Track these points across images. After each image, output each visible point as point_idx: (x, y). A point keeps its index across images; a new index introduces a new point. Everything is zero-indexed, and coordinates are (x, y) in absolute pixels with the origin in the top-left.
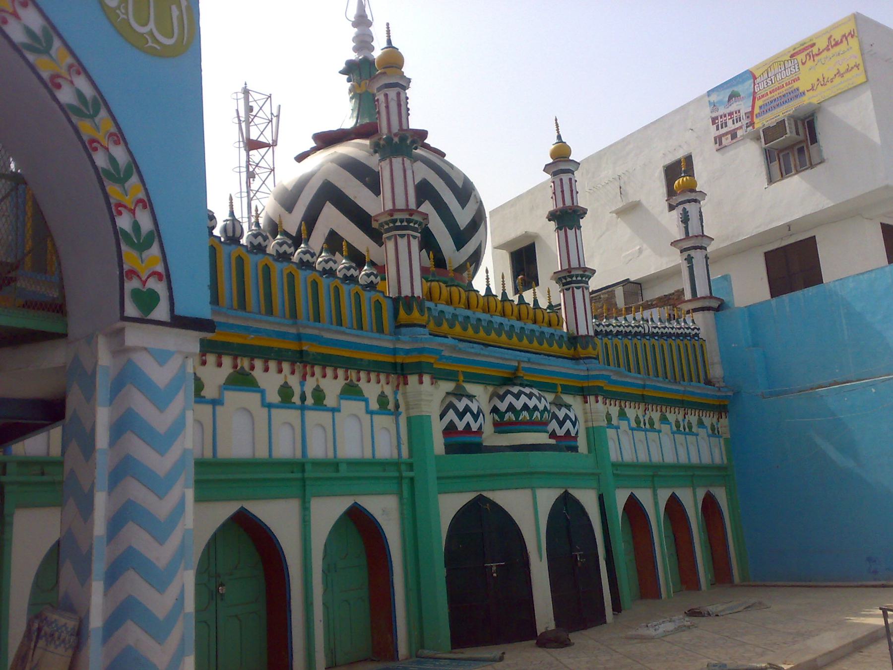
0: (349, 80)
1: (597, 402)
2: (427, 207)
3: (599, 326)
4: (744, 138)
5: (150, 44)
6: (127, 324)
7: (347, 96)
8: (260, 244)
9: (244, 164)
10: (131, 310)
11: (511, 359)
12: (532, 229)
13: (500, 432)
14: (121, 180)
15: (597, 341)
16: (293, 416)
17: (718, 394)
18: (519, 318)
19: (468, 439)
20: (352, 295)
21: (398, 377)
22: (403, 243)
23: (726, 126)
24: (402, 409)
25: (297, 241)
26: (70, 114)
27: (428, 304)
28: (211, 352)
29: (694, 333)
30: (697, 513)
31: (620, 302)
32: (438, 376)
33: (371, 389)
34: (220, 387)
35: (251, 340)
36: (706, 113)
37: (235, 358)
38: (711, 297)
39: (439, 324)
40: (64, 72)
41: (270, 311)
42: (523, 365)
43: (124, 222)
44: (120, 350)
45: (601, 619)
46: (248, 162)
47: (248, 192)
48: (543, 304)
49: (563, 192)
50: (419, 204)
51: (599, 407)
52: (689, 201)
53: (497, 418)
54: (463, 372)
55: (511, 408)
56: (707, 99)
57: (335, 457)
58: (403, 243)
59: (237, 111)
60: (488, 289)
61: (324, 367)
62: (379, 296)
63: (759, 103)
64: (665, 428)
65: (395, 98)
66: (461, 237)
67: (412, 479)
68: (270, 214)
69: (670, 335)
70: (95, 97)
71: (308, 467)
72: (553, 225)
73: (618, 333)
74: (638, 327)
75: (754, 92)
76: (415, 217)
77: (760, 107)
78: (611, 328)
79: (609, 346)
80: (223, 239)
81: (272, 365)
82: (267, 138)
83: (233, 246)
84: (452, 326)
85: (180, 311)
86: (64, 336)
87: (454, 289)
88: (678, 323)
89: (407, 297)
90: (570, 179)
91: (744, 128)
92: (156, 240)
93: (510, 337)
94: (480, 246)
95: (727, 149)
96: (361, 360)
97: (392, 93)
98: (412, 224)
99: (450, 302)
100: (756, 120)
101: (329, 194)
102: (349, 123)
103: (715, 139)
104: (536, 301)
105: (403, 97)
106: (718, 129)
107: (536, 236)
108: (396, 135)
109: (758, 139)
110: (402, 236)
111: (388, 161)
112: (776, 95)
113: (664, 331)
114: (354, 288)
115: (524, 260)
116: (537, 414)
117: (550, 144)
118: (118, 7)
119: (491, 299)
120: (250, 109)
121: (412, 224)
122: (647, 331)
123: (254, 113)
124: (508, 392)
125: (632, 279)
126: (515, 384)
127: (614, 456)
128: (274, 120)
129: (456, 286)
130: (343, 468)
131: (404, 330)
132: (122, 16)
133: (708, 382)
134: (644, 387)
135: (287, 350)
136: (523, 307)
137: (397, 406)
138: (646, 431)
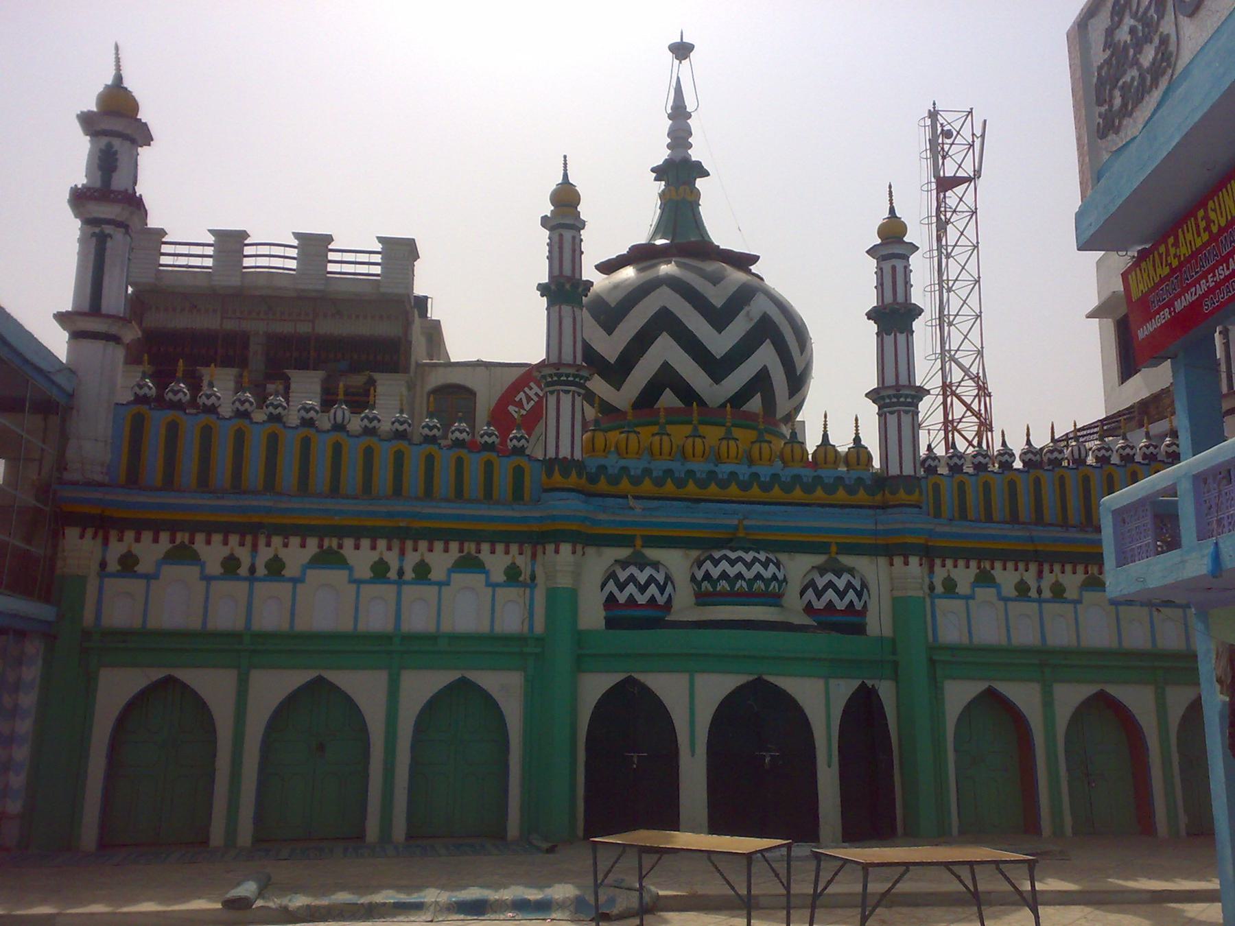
13: (705, 605)
16: (388, 591)
19: (650, 613)
24: (540, 579)
35: (337, 521)
55: (707, 576)
65: (570, 240)
82: (968, 170)
90: (574, 238)
98: (902, 399)
101: (665, 322)
137: (533, 578)
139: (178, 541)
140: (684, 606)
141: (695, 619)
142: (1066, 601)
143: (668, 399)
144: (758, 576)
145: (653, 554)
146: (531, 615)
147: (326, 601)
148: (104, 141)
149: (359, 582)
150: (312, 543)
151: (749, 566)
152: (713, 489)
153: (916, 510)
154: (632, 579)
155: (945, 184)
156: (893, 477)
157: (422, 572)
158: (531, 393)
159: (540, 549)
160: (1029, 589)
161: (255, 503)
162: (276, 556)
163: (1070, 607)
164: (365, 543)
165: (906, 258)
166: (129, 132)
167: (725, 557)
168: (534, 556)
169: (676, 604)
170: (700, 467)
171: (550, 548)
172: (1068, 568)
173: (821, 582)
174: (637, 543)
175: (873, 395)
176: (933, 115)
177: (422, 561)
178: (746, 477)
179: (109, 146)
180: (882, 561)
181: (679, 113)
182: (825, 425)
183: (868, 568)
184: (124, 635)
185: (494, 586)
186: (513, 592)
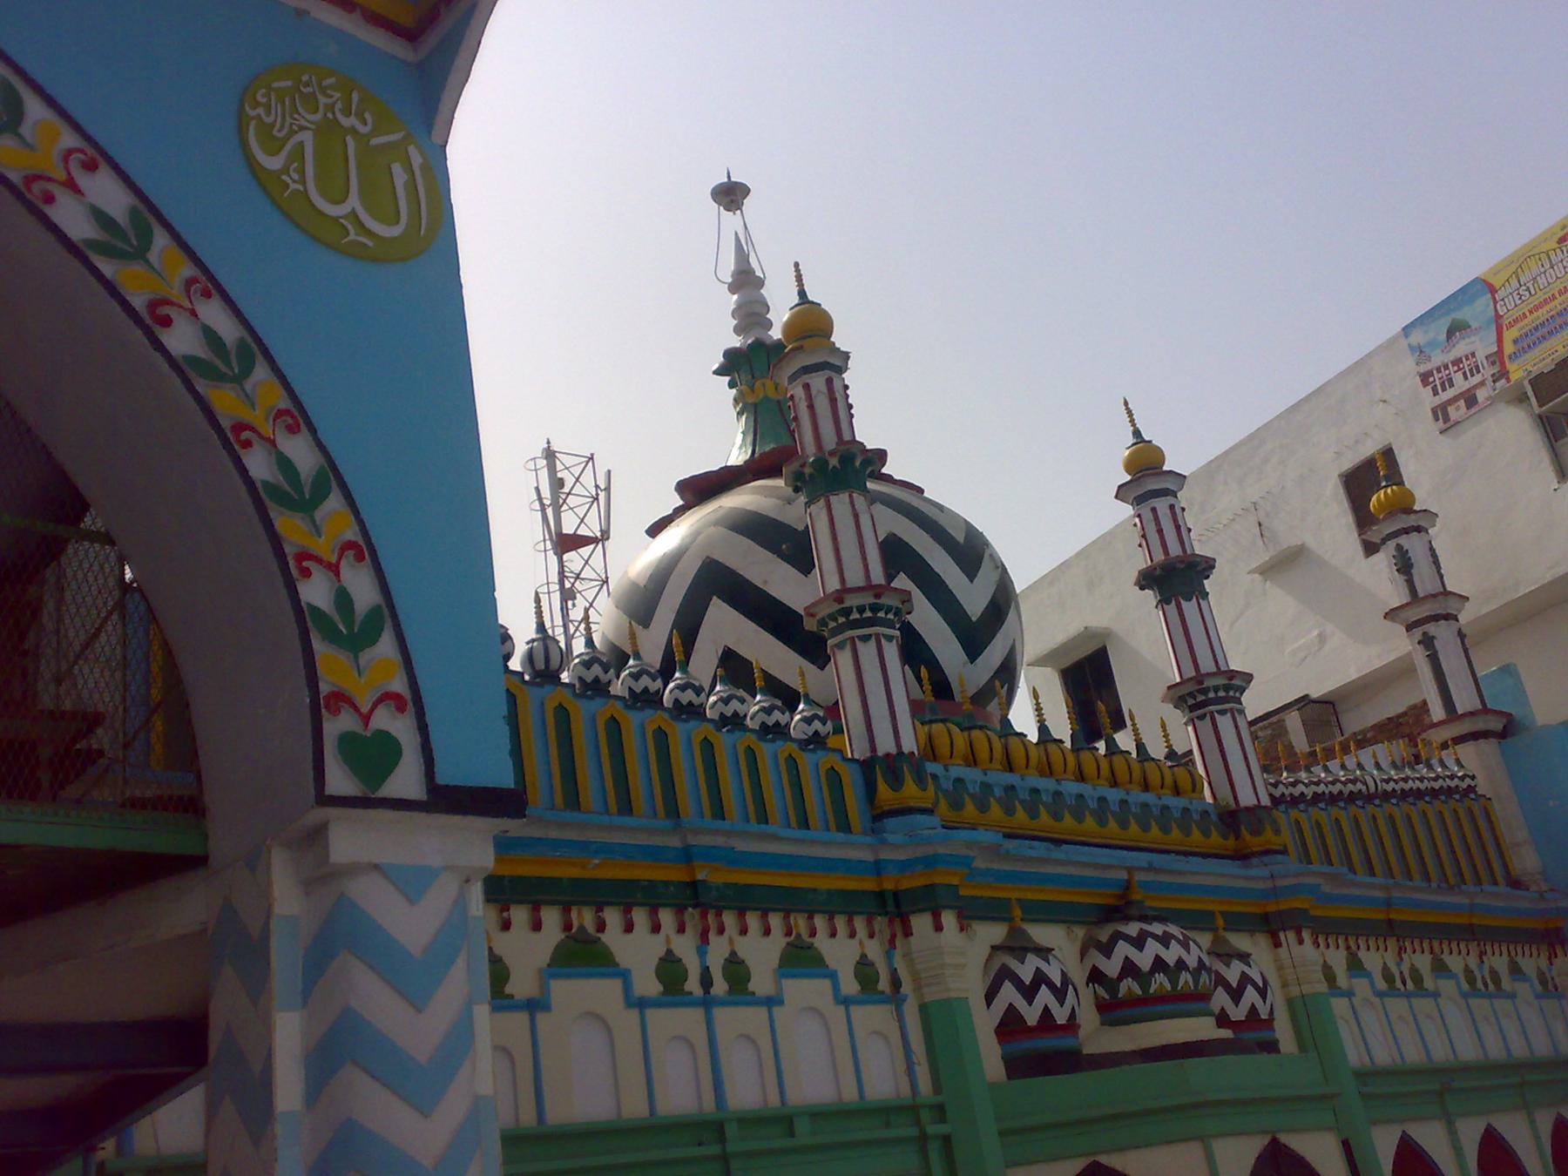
0: (731, 385)
1: (1301, 942)
2: (902, 582)
3: (1275, 785)
4: (1492, 401)
5: (352, 236)
6: (333, 812)
7: (733, 413)
8: (597, 680)
9: (554, 578)
10: (339, 781)
11: (1112, 866)
12: (1098, 621)
14: (305, 502)
15: (1279, 815)
16: (688, 1019)
17: (1542, 905)
18: (1114, 783)
20: (782, 761)
21: (891, 922)
22: (867, 652)
23: (1452, 385)
24: (906, 988)
25: (666, 673)
26: (191, 374)
27: (931, 767)
28: (521, 902)
29: (1464, 785)
30: (1545, 1166)
31: (1300, 741)
32: (970, 913)
33: (840, 950)
34: (540, 971)
36: (1409, 367)
37: (567, 910)
38: (1485, 710)
39: (957, 805)
40: (176, 292)
41: (626, 807)
42: (1140, 877)
43: (316, 592)
44: (322, 876)
46: (562, 573)
47: (565, 626)
48: (1157, 750)
49: (1160, 531)
50: (890, 577)
51: (1306, 953)
52: (1406, 531)
53: (1102, 992)
54: (1019, 900)
55: (1129, 968)
56: (1404, 343)
57: (783, 1103)
58: (867, 652)
59: (537, 489)
60: (1043, 729)
61: (741, 914)
62: (835, 759)
63: (1509, 335)
64: (1447, 986)
65: (824, 389)
66: (976, 635)
67: (947, 1140)
68: (611, 636)
69: (1419, 794)
70: (242, 340)
71: (731, 1130)
72: (1150, 596)
73: (1317, 797)
74: (1354, 781)
75: (1498, 317)
76: (886, 600)
77: (1515, 342)
78: (1301, 788)
79: (1306, 826)
80: (527, 678)
81: (640, 916)
82: (592, 528)
83: (548, 688)
84: (983, 807)
85: (443, 777)
86: (197, 862)
87: (976, 733)
88: (1430, 767)
89: (888, 755)
90: (1172, 507)
91: (1489, 383)
92: (388, 624)
93: (1102, 822)
94: (1013, 648)
95: (1458, 427)
96: (815, 890)
97: (818, 382)
98: (881, 614)
99: (972, 760)
100: (1511, 367)
101: (714, 582)
102: (737, 456)
103: (1434, 411)
104: (1140, 746)
105: (837, 385)
106: (1435, 393)
107: (1107, 634)
108: (832, 453)
109: (1522, 399)
111: (822, 502)
112: (1542, 314)
113: (1407, 786)
114: (784, 748)
115: (1090, 678)
116: (1185, 978)
117: (1122, 447)
118: (285, 170)
119: (1052, 747)
120: (557, 484)
121: (881, 614)
122: (1372, 789)
123: (566, 490)
124: (1117, 936)
125: (1315, 695)
126: (1127, 919)
127: (1354, 1056)
128: (602, 496)
129: (981, 728)
130: (802, 1126)
131: (891, 823)
132: (293, 186)
133: (1515, 884)
134: (1389, 903)
135: (667, 883)
136: (1117, 759)
137: (896, 983)
138: (1408, 995)
142: (753, 1000)
156: (1247, 809)
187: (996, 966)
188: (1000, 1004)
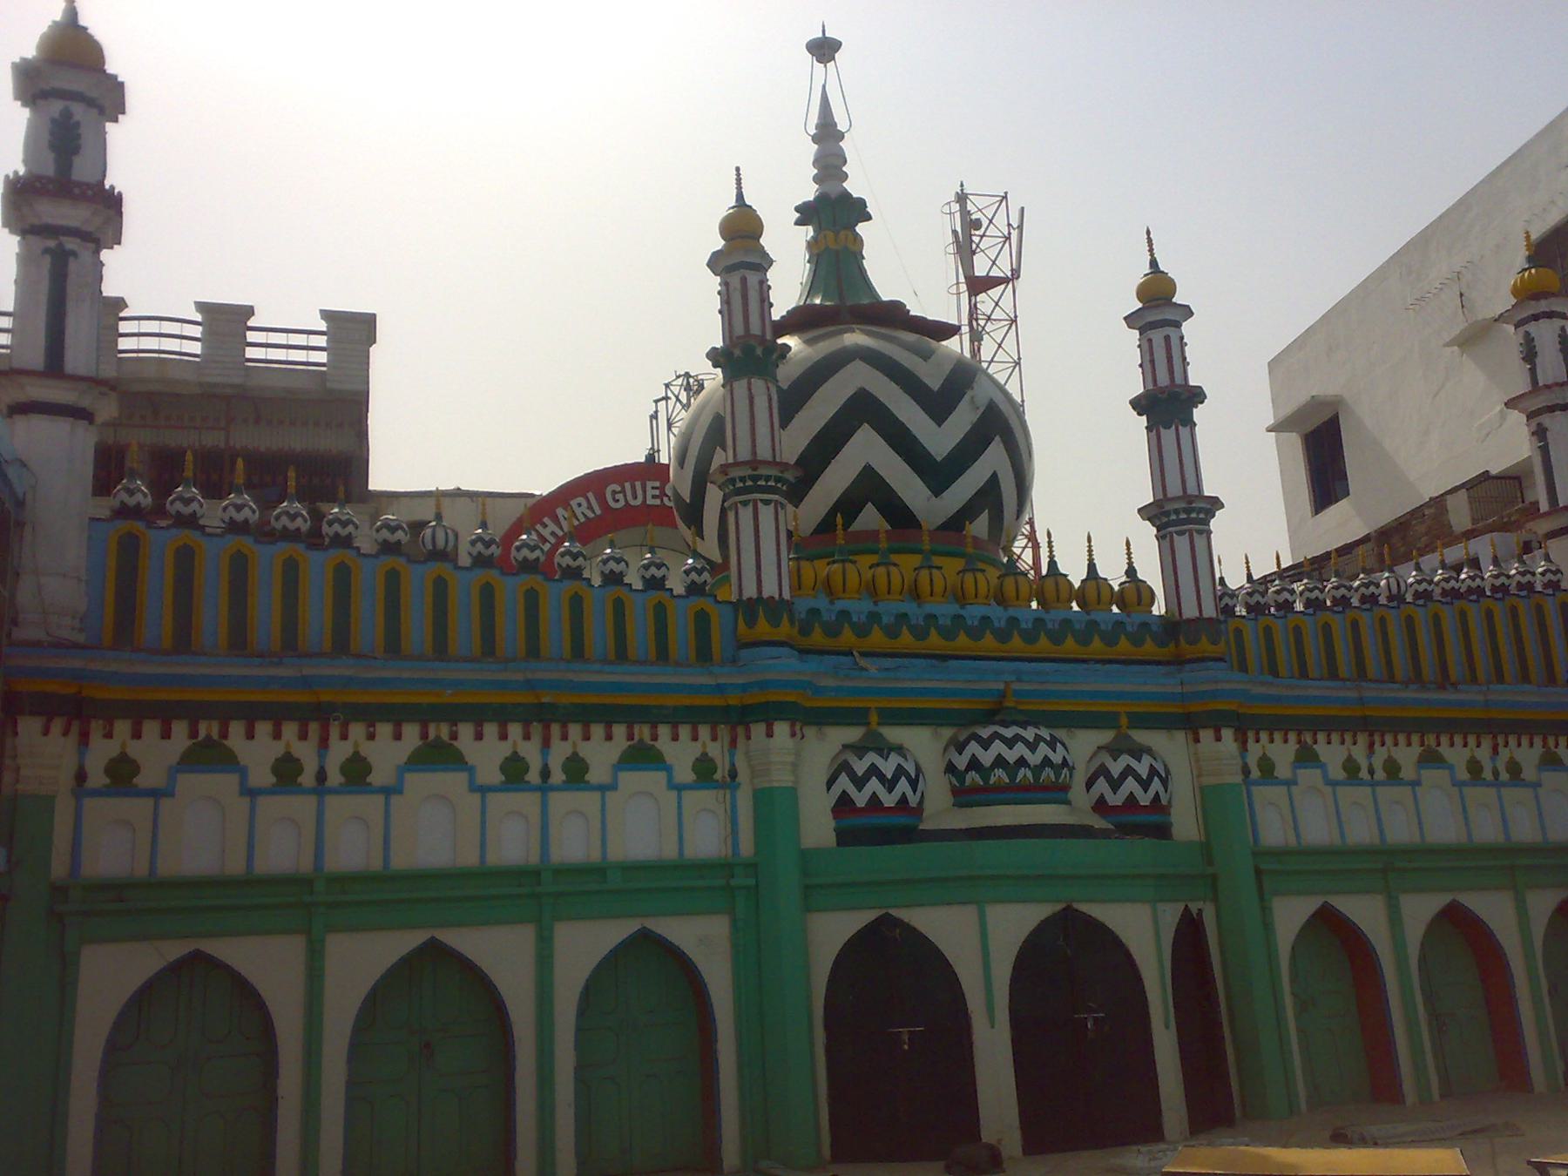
11: (991, 680)
16: (527, 802)
19: (901, 820)
24: (743, 777)
35: (448, 697)
45: (1149, 1130)
52: (1536, 318)
55: (974, 764)
65: (738, 286)
82: (1004, 268)
90: (1167, 339)
96: (660, 707)
98: (1194, 515)
110: (745, 504)
128: (1014, 234)
137: (733, 774)
139: (202, 734)
140: (939, 810)
141: (964, 826)
143: (870, 518)
144: (1047, 761)
145: (893, 734)
146: (735, 832)
147: (438, 820)
148: (56, 107)
149: (483, 790)
150: (411, 732)
151: (1033, 747)
152: (962, 640)
153: (1222, 665)
154: (874, 771)
155: (978, 285)
156: (1190, 621)
157: (576, 771)
158: (546, 533)
159: (741, 730)
160: (1359, 769)
161: (327, 672)
162: (356, 753)
163: (1407, 790)
164: (491, 729)
165: (1178, 325)
166: (94, 94)
167: (996, 736)
168: (733, 743)
169: (929, 808)
170: (945, 610)
171: (758, 729)
172: (1401, 738)
173: (1116, 768)
174: (869, 719)
175: (1146, 512)
176: (962, 198)
177: (575, 754)
178: (1003, 624)
179: (67, 114)
180: (1180, 736)
181: (828, 134)
182: (1090, 551)
183: (1170, 747)
184: (116, 889)
185: (679, 788)
186: (706, 797)
187: (1095, 765)
188: (837, 790)
